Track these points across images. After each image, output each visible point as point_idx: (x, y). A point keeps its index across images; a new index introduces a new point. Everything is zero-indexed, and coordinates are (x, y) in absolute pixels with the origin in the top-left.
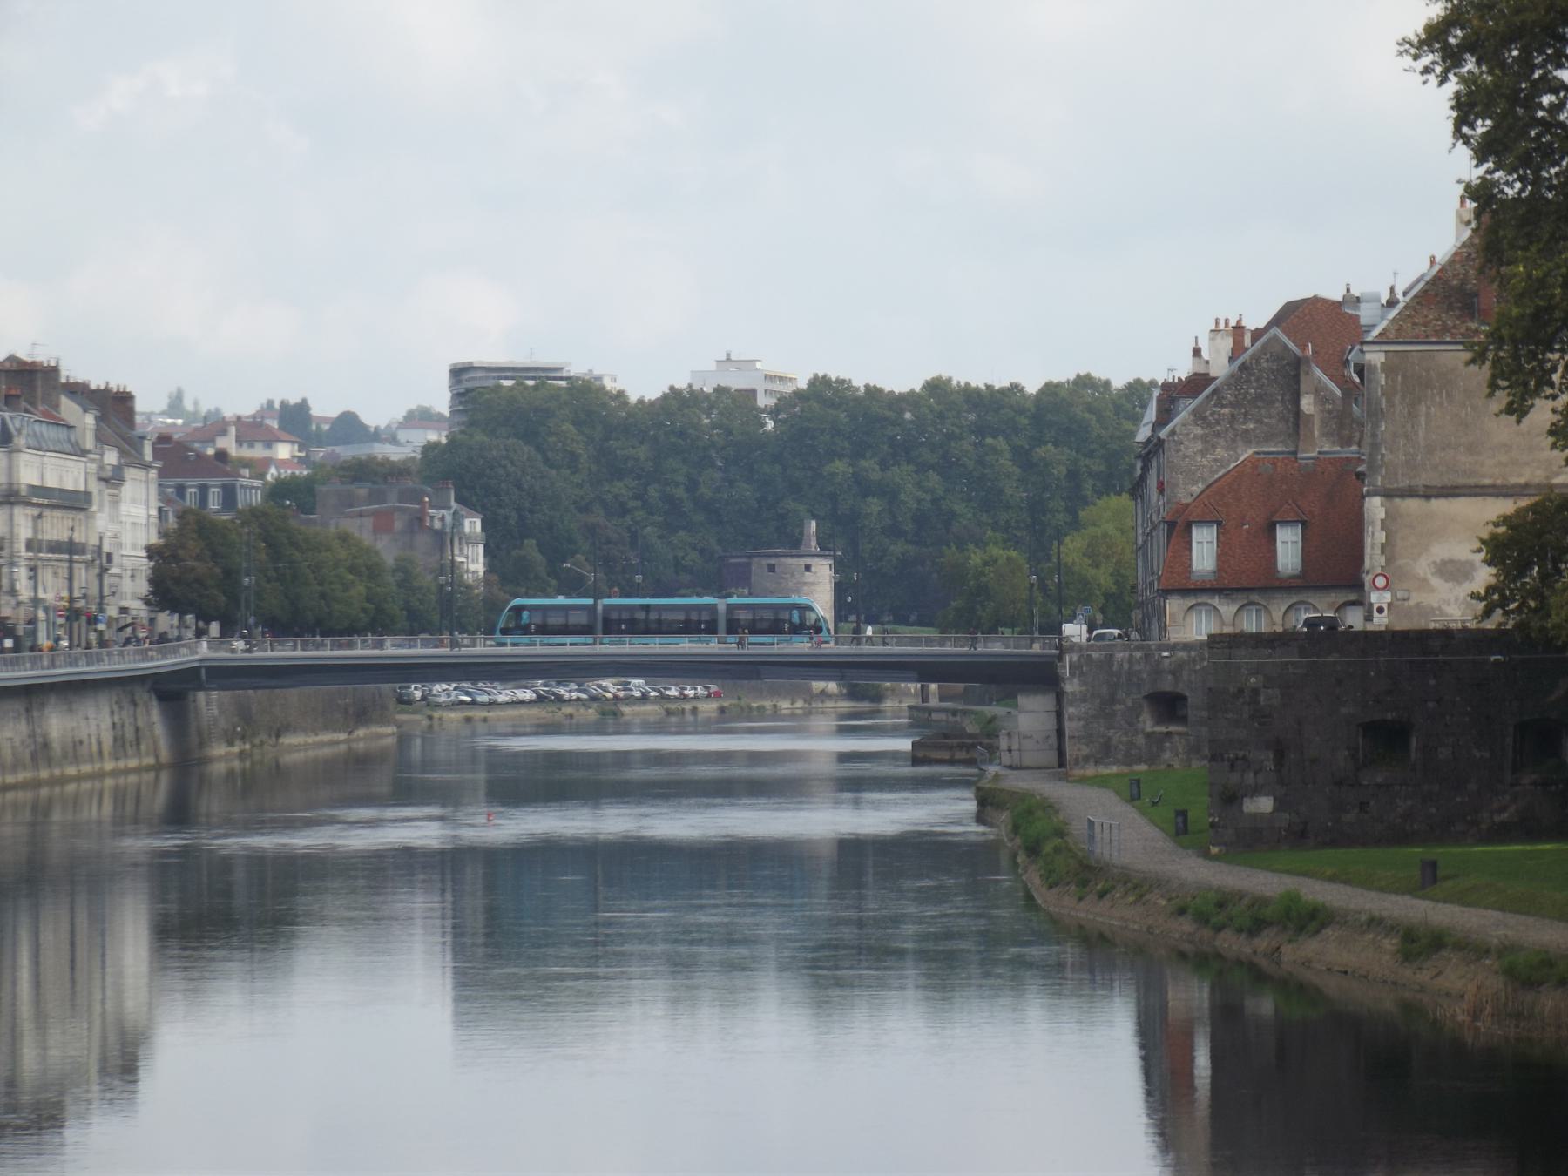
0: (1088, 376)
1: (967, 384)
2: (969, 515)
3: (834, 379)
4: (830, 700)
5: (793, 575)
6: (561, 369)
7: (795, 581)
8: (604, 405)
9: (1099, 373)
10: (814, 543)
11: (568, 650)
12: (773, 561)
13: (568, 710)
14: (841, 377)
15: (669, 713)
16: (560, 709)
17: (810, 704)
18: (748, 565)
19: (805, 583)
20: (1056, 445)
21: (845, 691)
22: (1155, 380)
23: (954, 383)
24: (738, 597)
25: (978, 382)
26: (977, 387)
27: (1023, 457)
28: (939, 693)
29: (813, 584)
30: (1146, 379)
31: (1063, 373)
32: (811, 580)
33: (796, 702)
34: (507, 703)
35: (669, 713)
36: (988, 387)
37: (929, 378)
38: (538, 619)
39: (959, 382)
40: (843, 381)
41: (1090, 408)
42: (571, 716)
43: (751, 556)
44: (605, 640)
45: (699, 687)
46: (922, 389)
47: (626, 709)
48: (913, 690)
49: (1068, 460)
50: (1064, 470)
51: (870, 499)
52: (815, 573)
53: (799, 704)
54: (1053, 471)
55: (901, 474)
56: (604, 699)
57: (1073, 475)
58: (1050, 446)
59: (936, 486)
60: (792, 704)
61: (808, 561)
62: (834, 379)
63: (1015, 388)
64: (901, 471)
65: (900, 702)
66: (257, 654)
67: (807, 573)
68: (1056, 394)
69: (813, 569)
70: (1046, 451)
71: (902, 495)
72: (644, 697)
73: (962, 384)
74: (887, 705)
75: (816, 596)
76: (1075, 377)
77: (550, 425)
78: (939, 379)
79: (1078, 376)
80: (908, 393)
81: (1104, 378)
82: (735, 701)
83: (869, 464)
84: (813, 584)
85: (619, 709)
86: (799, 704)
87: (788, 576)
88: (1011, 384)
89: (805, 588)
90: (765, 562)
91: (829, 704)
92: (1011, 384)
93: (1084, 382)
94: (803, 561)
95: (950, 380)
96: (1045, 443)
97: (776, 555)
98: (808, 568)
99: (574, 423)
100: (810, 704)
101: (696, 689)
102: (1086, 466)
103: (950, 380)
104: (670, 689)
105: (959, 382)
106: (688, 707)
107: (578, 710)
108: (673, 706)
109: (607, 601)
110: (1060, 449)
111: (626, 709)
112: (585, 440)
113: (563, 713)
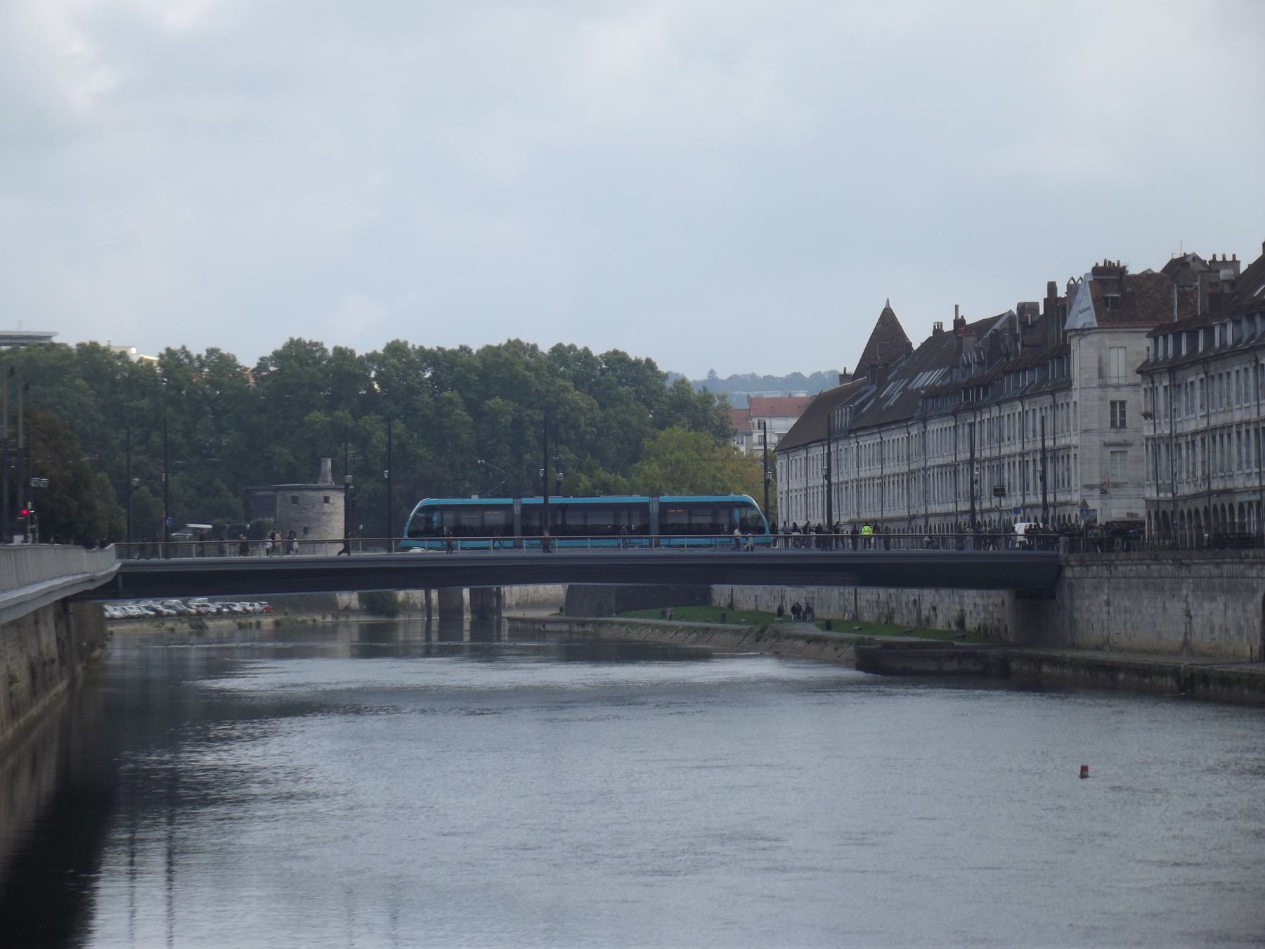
0: (517, 341)
1: (422, 348)
2: (430, 458)
3: (307, 342)
4: (353, 614)
5: (314, 506)
6: (49, 337)
7: (315, 511)
8: (111, 364)
9: (527, 339)
10: (330, 478)
11: (590, 552)
12: (296, 494)
13: (169, 625)
14: (314, 341)
15: (241, 626)
16: (163, 624)
17: (337, 618)
18: (273, 498)
19: (324, 513)
20: (503, 398)
21: (365, 607)
22: (573, 344)
23: (410, 346)
24: (735, 494)
25: (430, 345)
26: (432, 350)
27: (473, 408)
28: (440, 608)
29: (331, 514)
30: (566, 344)
31: (498, 340)
32: (329, 511)
33: (326, 616)
34: (123, 618)
35: (241, 626)
36: (439, 349)
37: (390, 341)
38: (449, 517)
39: (414, 346)
40: (316, 344)
41: (528, 367)
42: (172, 630)
43: (277, 490)
44: (663, 542)
45: (256, 604)
46: (384, 350)
47: (210, 624)
48: (419, 606)
49: (513, 410)
50: (509, 418)
51: (542, 418)
52: (333, 504)
53: (329, 619)
54: (502, 419)
55: (371, 421)
56: (189, 614)
57: (517, 423)
58: (498, 399)
59: (403, 433)
60: (324, 618)
61: (327, 493)
62: (307, 342)
63: (464, 349)
64: (372, 420)
65: (410, 616)
66: (354, 555)
67: (326, 504)
68: (499, 356)
69: (331, 501)
70: (495, 403)
71: (374, 440)
72: (219, 612)
73: (417, 347)
74: (401, 619)
75: (334, 524)
76: (506, 342)
77: (65, 380)
78: (397, 341)
79: (509, 341)
80: (371, 354)
81: (532, 342)
82: (284, 617)
83: (343, 414)
84: (331, 514)
85: (204, 623)
86: (329, 619)
87: (310, 507)
88: (461, 347)
89: (325, 517)
90: (289, 495)
91: (353, 619)
92: (461, 347)
93: (515, 347)
94: (322, 494)
95: (406, 343)
96: (494, 397)
97: (299, 489)
98: (326, 500)
99: (85, 379)
100: (337, 618)
101: (253, 605)
102: (527, 415)
103: (406, 343)
104: (235, 606)
105: (414, 346)
106: (253, 620)
107: (176, 625)
108: (243, 621)
109: (526, 501)
110: (506, 401)
111: (210, 624)
112: (96, 393)
113: (166, 628)
